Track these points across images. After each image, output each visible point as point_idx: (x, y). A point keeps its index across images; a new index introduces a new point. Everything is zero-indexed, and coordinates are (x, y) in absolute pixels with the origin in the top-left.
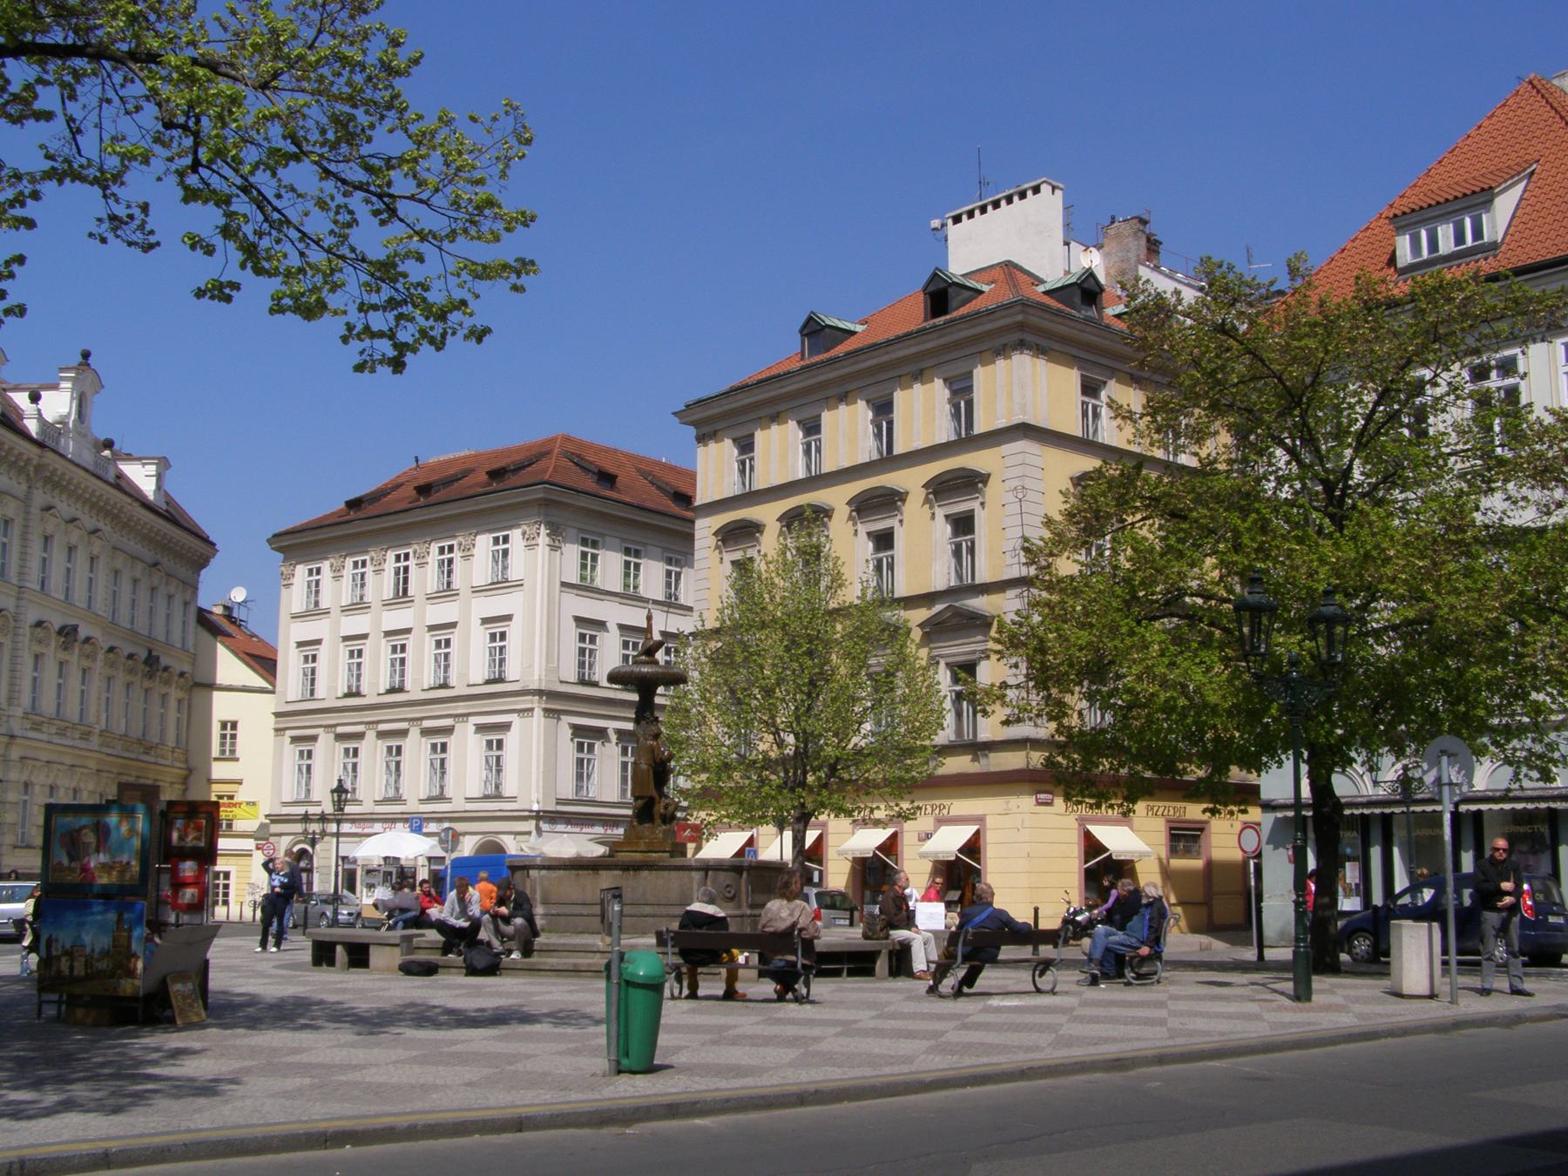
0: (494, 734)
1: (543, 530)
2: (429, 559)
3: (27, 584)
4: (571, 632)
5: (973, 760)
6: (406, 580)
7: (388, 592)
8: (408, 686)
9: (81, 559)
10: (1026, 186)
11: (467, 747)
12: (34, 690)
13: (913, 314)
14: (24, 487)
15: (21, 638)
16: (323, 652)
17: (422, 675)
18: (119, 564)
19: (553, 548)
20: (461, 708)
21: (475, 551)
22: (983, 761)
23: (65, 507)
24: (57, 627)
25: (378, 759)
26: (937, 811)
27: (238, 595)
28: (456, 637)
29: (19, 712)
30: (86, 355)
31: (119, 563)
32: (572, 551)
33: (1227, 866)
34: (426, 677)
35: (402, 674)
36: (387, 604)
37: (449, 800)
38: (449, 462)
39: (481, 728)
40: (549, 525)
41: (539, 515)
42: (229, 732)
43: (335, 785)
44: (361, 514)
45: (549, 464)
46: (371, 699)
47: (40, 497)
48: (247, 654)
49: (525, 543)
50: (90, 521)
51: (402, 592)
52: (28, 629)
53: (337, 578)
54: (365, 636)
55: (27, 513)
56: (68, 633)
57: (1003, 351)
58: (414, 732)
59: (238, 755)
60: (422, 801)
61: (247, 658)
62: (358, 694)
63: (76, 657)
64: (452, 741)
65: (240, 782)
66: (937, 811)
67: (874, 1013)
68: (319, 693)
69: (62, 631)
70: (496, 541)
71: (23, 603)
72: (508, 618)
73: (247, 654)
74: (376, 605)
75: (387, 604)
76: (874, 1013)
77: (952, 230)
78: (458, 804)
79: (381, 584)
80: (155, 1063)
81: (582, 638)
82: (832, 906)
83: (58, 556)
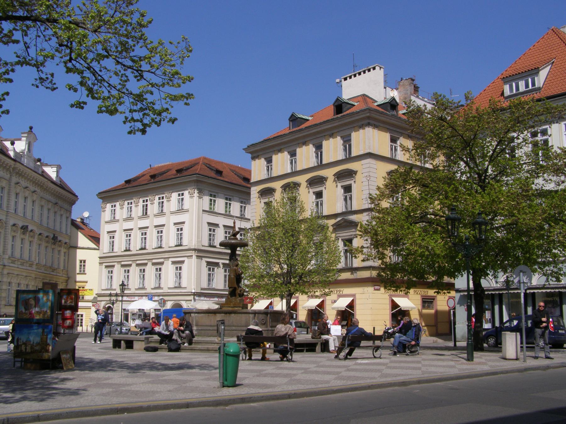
0: (178, 265)
1: (196, 191)
2: (155, 202)
3: (10, 211)
4: (206, 228)
5: (351, 274)
6: (146, 209)
7: (140, 214)
8: (147, 247)
9: (29, 201)
10: (370, 67)
11: (169, 269)
12: (12, 249)
13: (330, 113)
14: (9, 176)
15: (8, 230)
16: (117, 235)
17: (152, 243)
18: (43, 203)
19: (200, 198)
20: (166, 255)
21: (171, 199)
22: (355, 274)
23: (24, 183)
24: (20, 226)
25: (137, 274)
26: (338, 293)
27: (86, 214)
28: (164, 229)
29: (7, 257)
30: (31, 128)
31: (43, 203)
32: (207, 199)
33: (443, 312)
34: (154, 244)
35: (145, 243)
36: (140, 218)
37: (162, 288)
38: (162, 166)
39: (173, 263)
40: (198, 189)
41: (195, 186)
42: (83, 264)
44: (130, 185)
45: (198, 167)
46: (134, 252)
47: (15, 179)
48: (89, 236)
49: (189, 196)
50: (32, 188)
51: (145, 214)
52: (10, 227)
53: (122, 208)
54: (132, 229)
55: (10, 185)
56: (24, 228)
58: (150, 264)
59: (86, 272)
60: (152, 289)
61: (89, 237)
62: (129, 250)
63: (27, 237)
64: (163, 267)
65: (86, 282)
66: (338, 293)
67: (315, 365)
68: (115, 250)
69: (22, 228)
70: (179, 195)
71: (8, 217)
72: (183, 223)
73: (89, 236)
74: (136, 218)
75: (140, 218)
76: (315, 365)
77: (344, 83)
78: (165, 290)
79: (138, 211)
80: (56, 383)
81: (210, 230)
83: (21, 201)
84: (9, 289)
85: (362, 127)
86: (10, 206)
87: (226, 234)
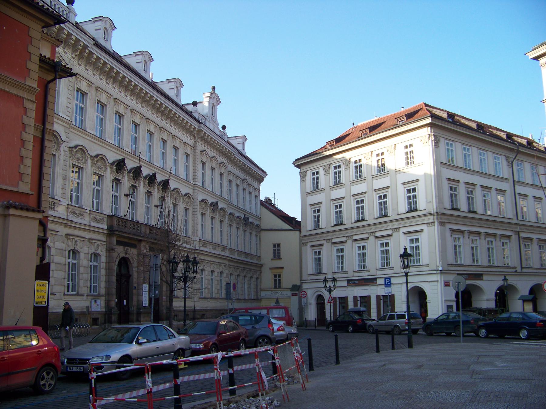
3: (197, 183)
4: (446, 185)
7: (353, 177)
9: (217, 173)
12: (202, 230)
14: (193, 141)
15: (196, 204)
18: (231, 178)
20: (396, 225)
23: (212, 153)
24: (210, 202)
29: (197, 239)
30: (214, 88)
31: (231, 178)
38: (364, 124)
42: (277, 248)
43: (402, 252)
47: (201, 146)
50: (220, 159)
52: (198, 203)
55: (195, 152)
56: (214, 205)
58: (372, 239)
59: (281, 257)
61: (281, 217)
62: (341, 224)
63: (218, 216)
65: (282, 268)
69: (211, 204)
71: (196, 191)
73: (281, 216)
75: (331, 188)
81: (451, 188)
83: (208, 172)
84: (95, 267)
85: (226, 292)
86: (197, 168)
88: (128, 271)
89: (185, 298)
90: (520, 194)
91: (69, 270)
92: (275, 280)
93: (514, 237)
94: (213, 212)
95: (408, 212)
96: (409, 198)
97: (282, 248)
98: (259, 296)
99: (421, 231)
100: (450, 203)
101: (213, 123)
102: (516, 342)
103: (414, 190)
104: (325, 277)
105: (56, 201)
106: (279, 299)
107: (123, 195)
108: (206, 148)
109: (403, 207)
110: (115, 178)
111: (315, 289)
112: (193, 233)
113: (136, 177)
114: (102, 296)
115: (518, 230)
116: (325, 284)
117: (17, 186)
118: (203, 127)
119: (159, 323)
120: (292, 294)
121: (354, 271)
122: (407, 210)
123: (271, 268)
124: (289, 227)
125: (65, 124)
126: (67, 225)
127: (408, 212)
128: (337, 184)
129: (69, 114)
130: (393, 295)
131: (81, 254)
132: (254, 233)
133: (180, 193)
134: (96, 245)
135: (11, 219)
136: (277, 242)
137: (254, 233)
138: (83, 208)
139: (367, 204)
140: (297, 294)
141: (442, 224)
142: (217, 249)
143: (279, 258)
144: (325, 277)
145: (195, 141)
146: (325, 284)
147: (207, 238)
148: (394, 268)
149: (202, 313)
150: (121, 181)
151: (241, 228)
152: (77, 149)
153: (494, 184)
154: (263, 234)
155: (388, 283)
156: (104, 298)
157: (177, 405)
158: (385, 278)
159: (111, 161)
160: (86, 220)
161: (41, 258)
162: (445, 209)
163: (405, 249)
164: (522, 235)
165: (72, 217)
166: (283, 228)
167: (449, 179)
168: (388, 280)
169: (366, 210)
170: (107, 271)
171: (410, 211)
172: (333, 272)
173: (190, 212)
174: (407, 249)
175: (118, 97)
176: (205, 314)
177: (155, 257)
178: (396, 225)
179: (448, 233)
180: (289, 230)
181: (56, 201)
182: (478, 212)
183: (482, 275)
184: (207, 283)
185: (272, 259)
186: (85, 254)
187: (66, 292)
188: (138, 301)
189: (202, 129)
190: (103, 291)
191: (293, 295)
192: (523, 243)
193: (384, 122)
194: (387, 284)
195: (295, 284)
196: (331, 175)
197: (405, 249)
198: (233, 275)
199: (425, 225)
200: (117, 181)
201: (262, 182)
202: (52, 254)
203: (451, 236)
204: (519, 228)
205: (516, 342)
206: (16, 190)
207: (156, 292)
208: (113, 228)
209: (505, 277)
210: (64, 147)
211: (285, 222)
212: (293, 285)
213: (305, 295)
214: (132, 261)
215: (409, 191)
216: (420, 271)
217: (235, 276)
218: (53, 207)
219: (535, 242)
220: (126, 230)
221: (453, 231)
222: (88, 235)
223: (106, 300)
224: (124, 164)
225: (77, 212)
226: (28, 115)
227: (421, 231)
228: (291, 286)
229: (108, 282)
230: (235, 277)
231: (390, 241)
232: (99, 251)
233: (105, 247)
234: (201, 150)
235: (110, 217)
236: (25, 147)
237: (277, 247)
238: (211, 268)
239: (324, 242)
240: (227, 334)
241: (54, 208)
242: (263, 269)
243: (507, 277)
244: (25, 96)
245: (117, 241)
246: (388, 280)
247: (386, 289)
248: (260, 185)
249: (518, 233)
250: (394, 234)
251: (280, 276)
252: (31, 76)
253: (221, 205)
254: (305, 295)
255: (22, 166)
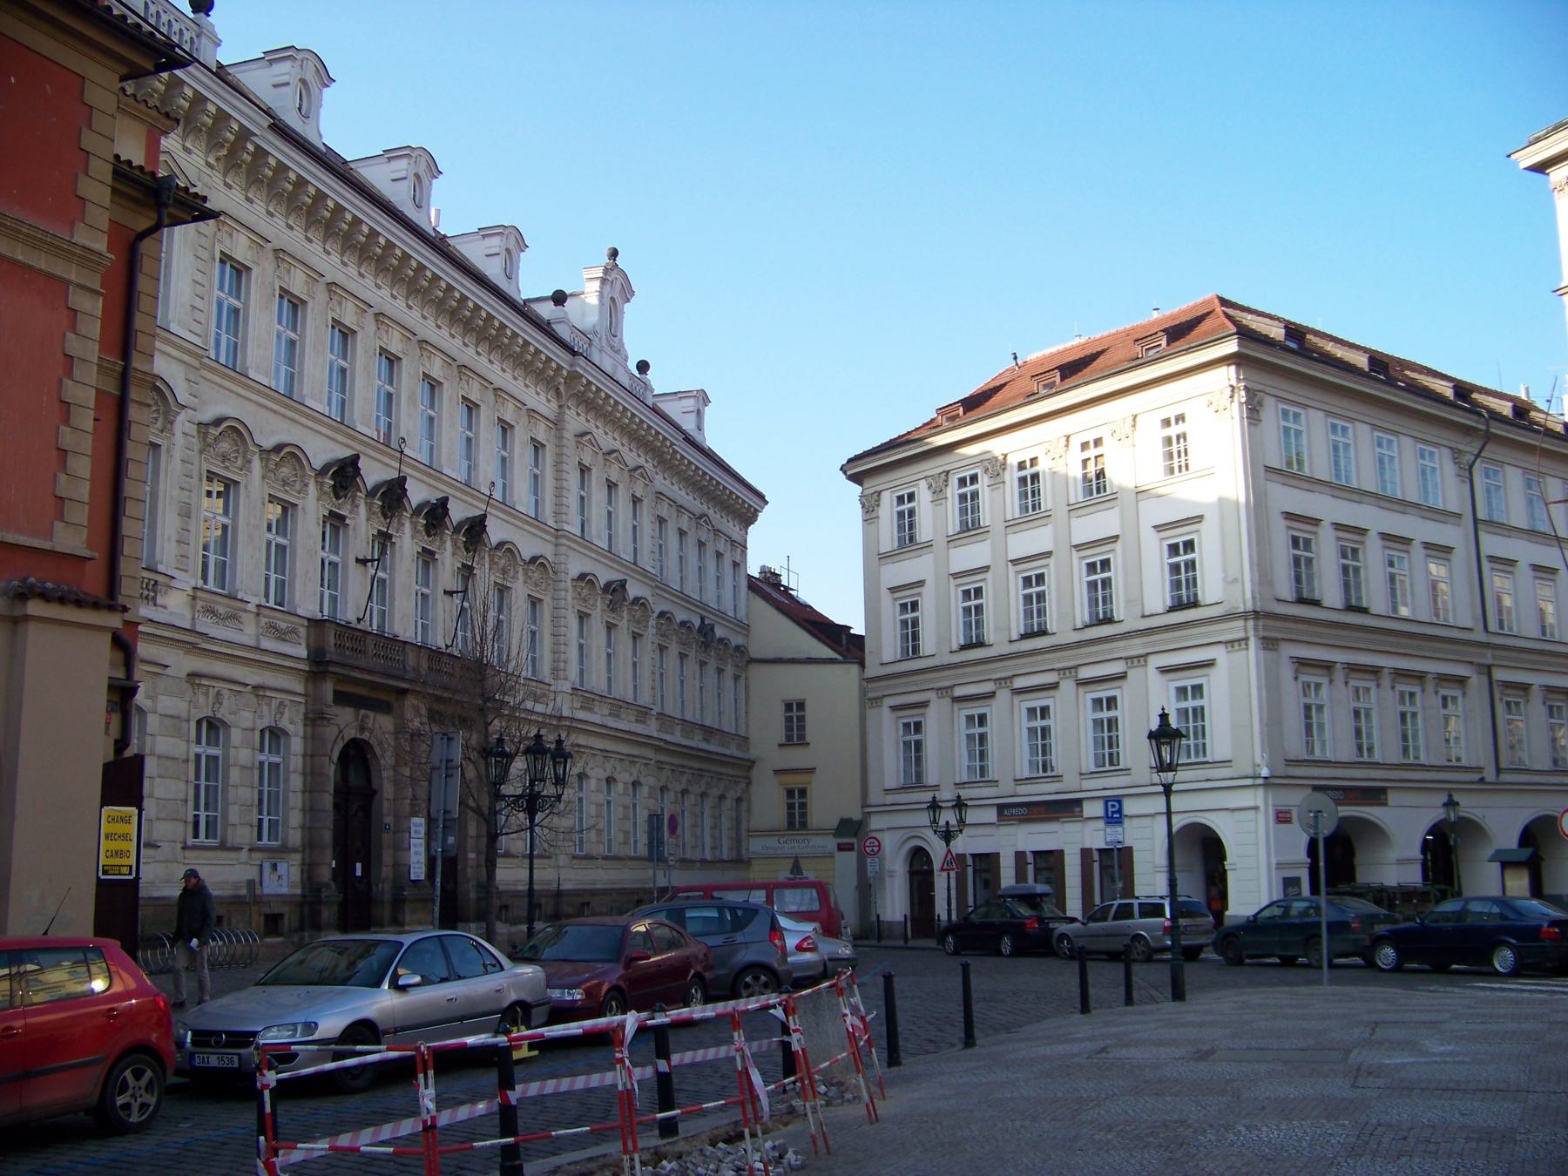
3: (566, 527)
4: (1280, 533)
7: (1013, 508)
9: (623, 496)
12: (581, 662)
14: (554, 405)
15: (562, 585)
18: (664, 510)
20: (1136, 647)
23: (608, 439)
24: (603, 582)
29: (567, 687)
30: (614, 254)
31: (664, 510)
38: (1045, 358)
42: (795, 714)
47: (576, 420)
50: (633, 457)
52: (569, 583)
55: (561, 438)
56: (615, 590)
57: (649, 838)
58: (1067, 686)
59: (808, 739)
61: (806, 625)
62: (980, 644)
63: (625, 620)
65: (811, 771)
69: (607, 588)
71: (563, 549)
73: (806, 621)
75: (951, 541)
81: (1295, 542)
82: (782, 950)
83: (598, 494)
84: (274, 767)
87: (791, 710)
88: (369, 780)
89: (531, 857)
90: (1492, 559)
91: (198, 777)
92: (791, 806)
93: (1476, 682)
94: (613, 610)
95: (1172, 609)
96: (1175, 568)
97: (809, 713)
98: (744, 852)
99: (1209, 664)
100: (1294, 585)
101: (612, 354)
102: (1481, 985)
103: (1189, 546)
104: (934, 798)
105: (160, 579)
106: (801, 861)
107: (352, 562)
108: (591, 426)
109: (1157, 595)
110: (331, 512)
111: (904, 831)
112: (555, 671)
113: (390, 508)
114: (294, 850)
115: (1489, 661)
116: (934, 817)
117: (49, 535)
118: (584, 365)
119: (456, 930)
120: (839, 845)
121: (1016, 780)
122: (1169, 603)
123: (777, 772)
124: (831, 654)
125: (186, 358)
126: (193, 648)
127: (1172, 609)
128: (969, 530)
129: (197, 328)
130: (1130, 849)
131: (233, 731)
132: (730, 671)
133: (517, 554)
134: (274, 704)
135: (33, 630)
136: (794, 695)
137: (730, 671)
138: (239, 597)
139: (1053, 586)
140: (852, 844)
141: (1268, 643)
142: (623, 716)
143: (802, 742)
144: (934, 798)
145: (560, 407)
146: (934, 817)
147: (594, 684)
148: (1132, 772)
149: (581, 900)
150: (347, 521)
151: (692, 655)
152: (220, 430)
153: (1419, 529)
154: (756, 672)
155: (1113, 813)
156: (298, 857)
157: (508, 1163)
158: (1107, 800)
159: (318, 463)
160: (247, 633)
161: (116, 742)
162: (1278, 600)
163: (1164, 717)
164: (1500, 675)
165: (206, 625)
166: (813, 655)
167: (1289, 516)
168: (1113, 806)
169: (1051, 604)
170: (309, 778)
171: (1177, 606)
172: (958, 781)
173: (546, 611)
174: (1170, 717)
175: (340, 278)
176: (588, 904)
177: (445, 740)
178: (1136, 647)
179: (1287, 671)
180: (831, 661)
181: (160, 579)
182: (1373, 611)
183: (1383, 790)
184: (594, 814)
185: (780, 745)
186: (243, 729)
187: (191, 841)
188: (396, 865)
189: (581, 372)
190: (295, 838)
191: (841, 848)
192: (1501, 699)
193: (1103, 352)
194: (1112, 817)
195: (846, 816)
196: (949, 502)
197: (1164, 717)
198: (668, 789)
199: (1221, 648)
200: (336, 521)
201: (752, 523)
202: (149, 729)
203: (1296, 678)
204: (1489, 655)
205: (1481, 985)
206: (47, 545)
207: (447, 839)
208: (324, 655)
209: (1450, 796)
210: (182, 423)
211: (819, 639)
212: (841, 819)
213: (876, 849)
214: (378, 751)
215: (1174, 549)
216: (1207, 780)
217: (676, 792)
218: (152, 594)
219: (1536, 697)
220: (363, 663)
221: (1302, 663)
222: (253, 676)
223: (303, 864)
224: (357, 470)
225: (221, 610)
226: (82, 329)
227: (1209, 664)
228: (834, 823)
229: (311, 810)
230: (676, 797)
231: (1120, 692)
232: (285, 723)
233: (302, 709)
234: (578, 432)
235: (315, 624)
236: (72, 422)
237: (795, 711)
238: (605, 770)
239: (931, 696)
240: (652, 960)
241: (154, 599)
242: (755, 772)
243: (1456, 798)
244: (73, 277)
245: (336, 692)
246: (1113, 806)
247: (1108, 830)
248: (747, 533)
249: (1488, 670)
250: (1131, 673)
251: (803, 793)
252: (88, 219)
253: (633, 590)
254: (876, 849)
255: (62, 478)
